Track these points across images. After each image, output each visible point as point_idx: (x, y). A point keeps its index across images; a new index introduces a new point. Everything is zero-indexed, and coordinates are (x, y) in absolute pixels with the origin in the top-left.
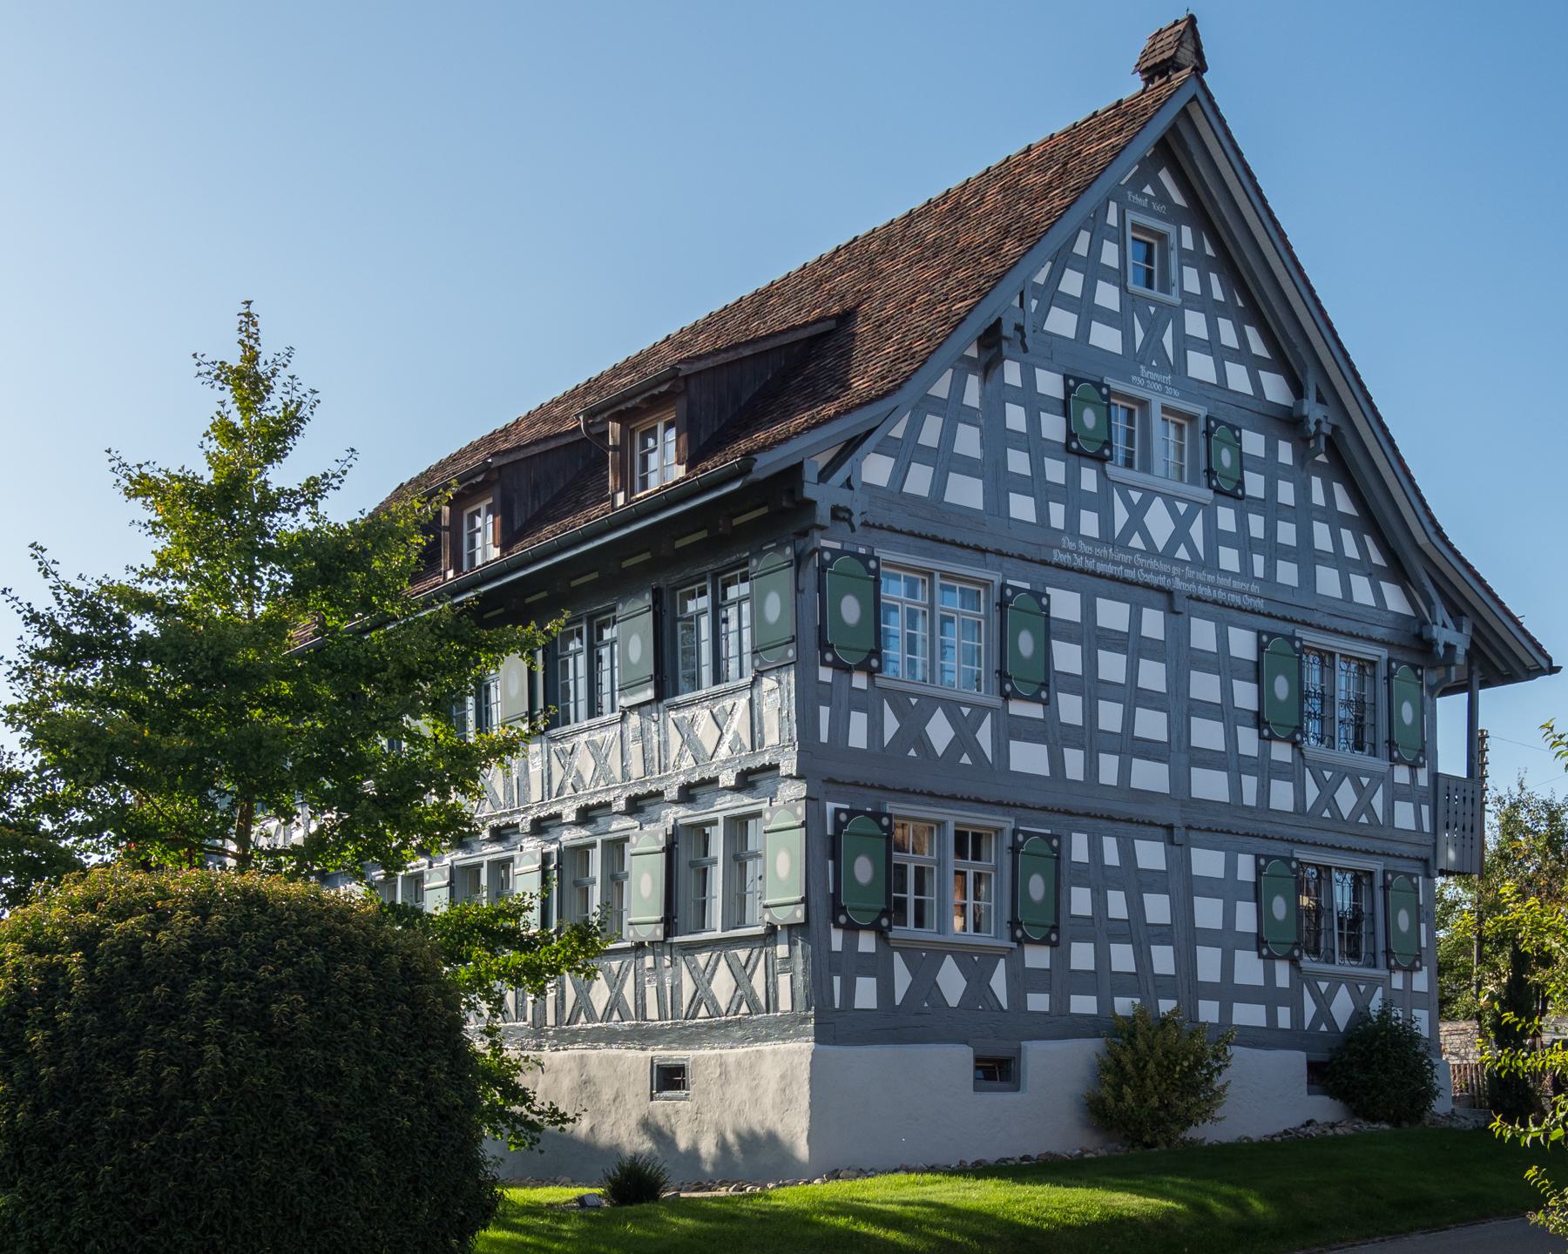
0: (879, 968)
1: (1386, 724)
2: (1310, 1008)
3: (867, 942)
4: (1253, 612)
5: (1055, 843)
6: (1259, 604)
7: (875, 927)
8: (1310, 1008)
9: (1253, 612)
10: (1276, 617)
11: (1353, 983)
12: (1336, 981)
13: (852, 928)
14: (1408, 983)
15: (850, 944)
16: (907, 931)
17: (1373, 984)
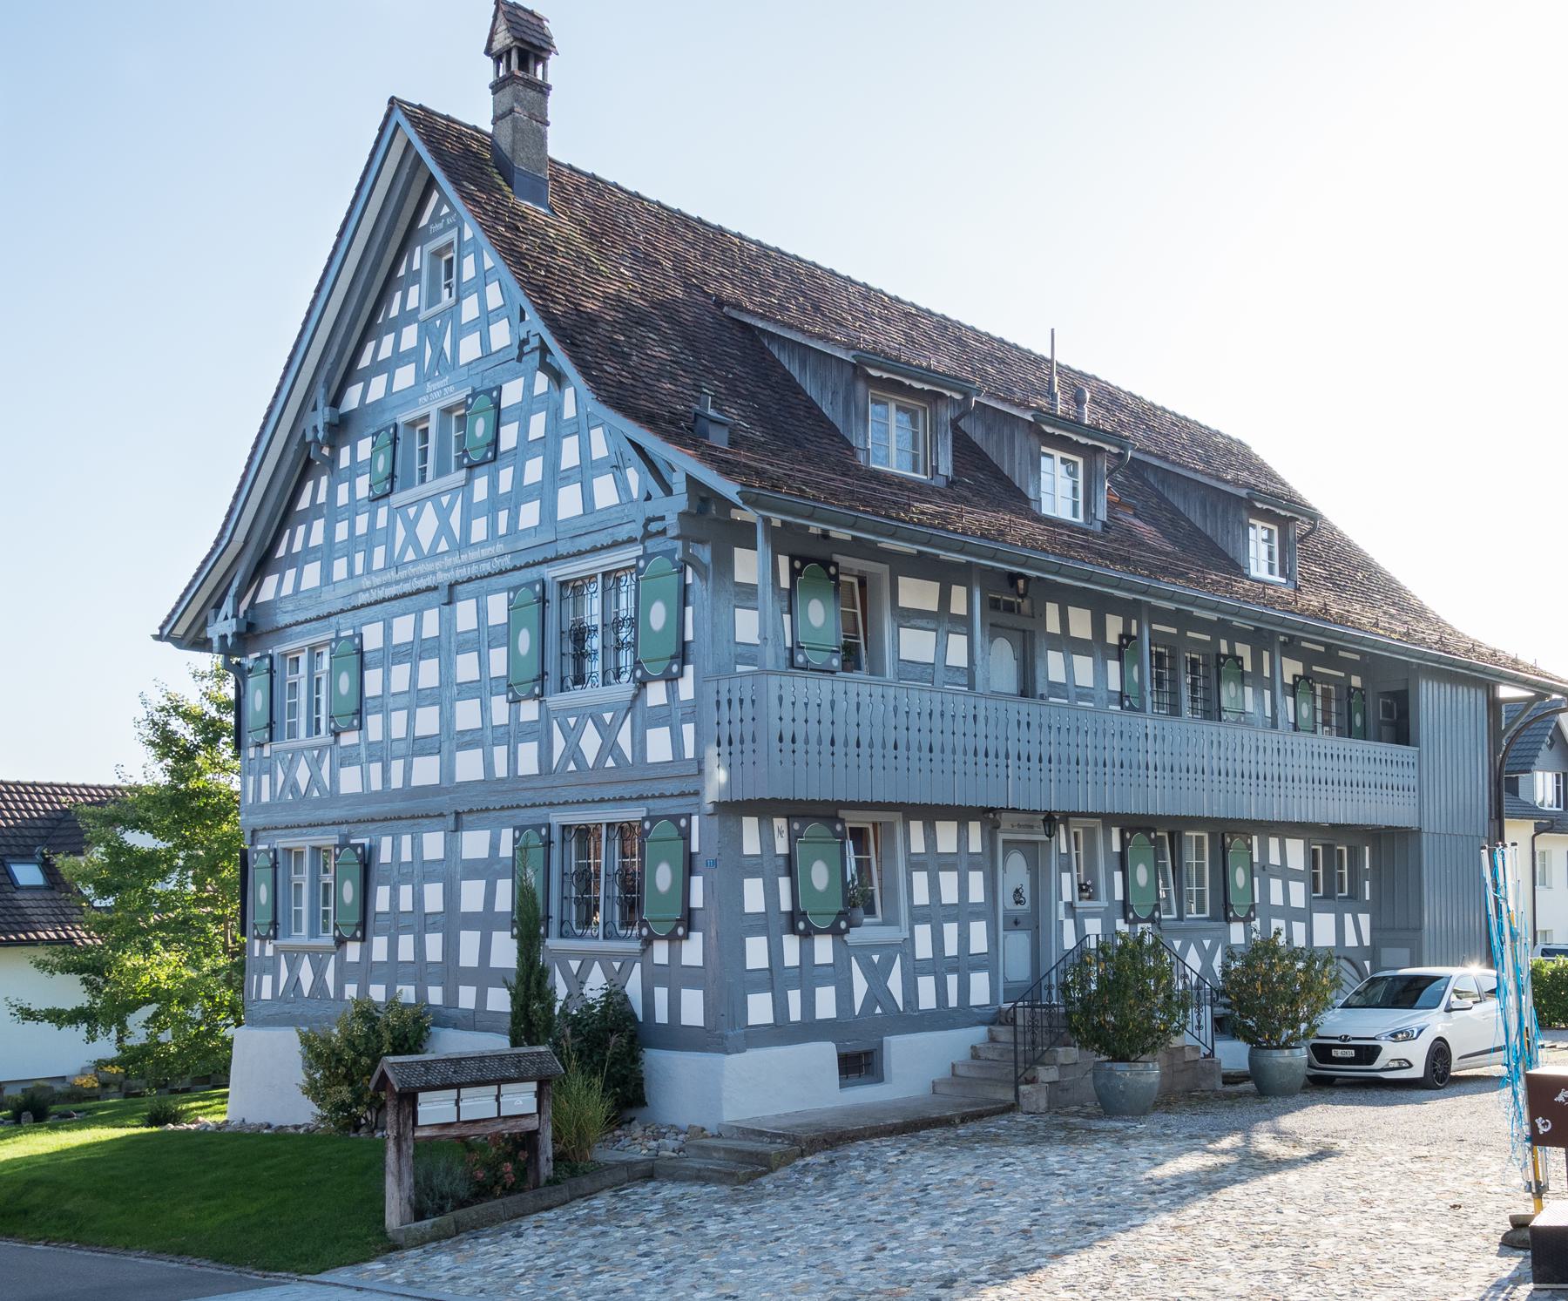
0: (839, 977)
1: (547, 646)
2: (860, 987)
3: (824, 950)
4: (501, 573)
5: (683, 823)
6: (507, 562)
7: (835, 931)
8: (860, 987)
9: (501, 573)
10: (521, 568)
11: (605, 958)
12: (587, 960)
13: (807, 935)
14: (675, 955)
15: (807, 953)
16: (867, 932)
17: (627, 961)
